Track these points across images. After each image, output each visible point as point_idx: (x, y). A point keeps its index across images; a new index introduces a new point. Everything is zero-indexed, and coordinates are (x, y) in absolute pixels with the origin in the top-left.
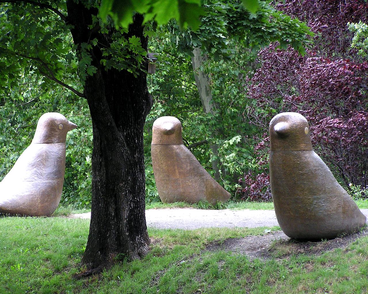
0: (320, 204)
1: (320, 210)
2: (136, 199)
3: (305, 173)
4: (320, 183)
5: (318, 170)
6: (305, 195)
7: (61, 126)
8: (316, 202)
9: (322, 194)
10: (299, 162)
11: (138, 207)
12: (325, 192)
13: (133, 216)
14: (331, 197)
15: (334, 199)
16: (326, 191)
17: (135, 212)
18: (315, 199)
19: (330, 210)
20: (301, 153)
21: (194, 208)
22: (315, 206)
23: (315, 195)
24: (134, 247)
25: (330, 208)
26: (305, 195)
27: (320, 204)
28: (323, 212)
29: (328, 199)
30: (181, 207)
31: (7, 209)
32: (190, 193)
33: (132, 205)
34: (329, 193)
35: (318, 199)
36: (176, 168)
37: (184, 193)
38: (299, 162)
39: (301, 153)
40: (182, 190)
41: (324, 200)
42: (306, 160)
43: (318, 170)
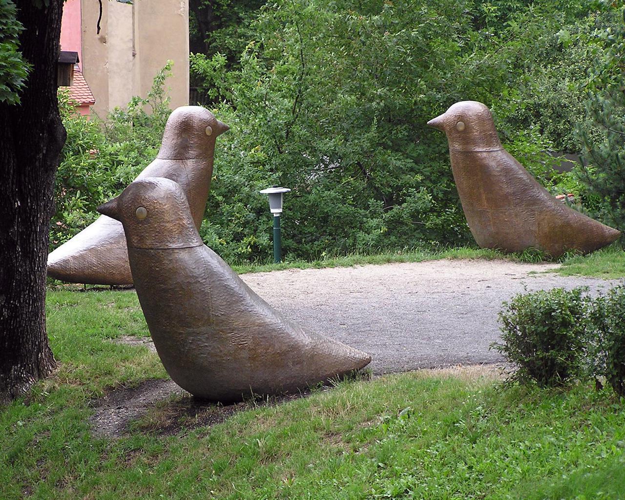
0: (199, 343)
1: (202, 354)
2: (12, 304)
3: (170, 289)
4: (198, 306)
5: (196, 283)
6: (174, 327)
7: (210, 130)
8: (193, 340)
9: (203, 325)
10: (157, 269)
11: (16, 317)
12: (208, 323)
13: (7, 332)
14: (223, 332)
15: (230, 335)
16: (211, 321)
17: (10, 325)
18: (189, 334)
19: (220, 354)
20: (161, 253)
21: (513, 260)
22: (192, 346)
23: (190, 327)
24: (7, 384)
25: (221, 351)
26: (174, 327)
27: (199, 343)
28: (206, 357)
29: (215, 335)
30: (489, 258)
31: (68, 273)
32: (508, 234)
33: (6, 313)
34: (217, 325)
35: (195, 334)
36: (482, 191)
37: (497, 233)
38: (157, 269)
39: (161, 253)
40: (492, 229)
41: (206, 335)
42: (170, 266)
43: (196, 283)
